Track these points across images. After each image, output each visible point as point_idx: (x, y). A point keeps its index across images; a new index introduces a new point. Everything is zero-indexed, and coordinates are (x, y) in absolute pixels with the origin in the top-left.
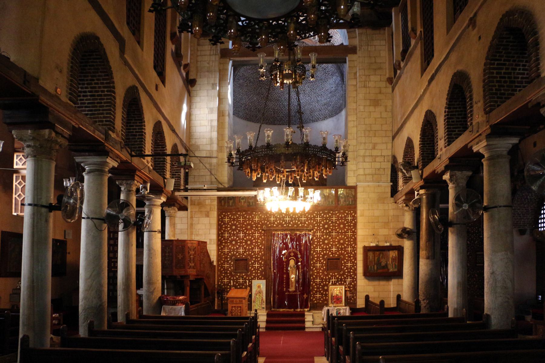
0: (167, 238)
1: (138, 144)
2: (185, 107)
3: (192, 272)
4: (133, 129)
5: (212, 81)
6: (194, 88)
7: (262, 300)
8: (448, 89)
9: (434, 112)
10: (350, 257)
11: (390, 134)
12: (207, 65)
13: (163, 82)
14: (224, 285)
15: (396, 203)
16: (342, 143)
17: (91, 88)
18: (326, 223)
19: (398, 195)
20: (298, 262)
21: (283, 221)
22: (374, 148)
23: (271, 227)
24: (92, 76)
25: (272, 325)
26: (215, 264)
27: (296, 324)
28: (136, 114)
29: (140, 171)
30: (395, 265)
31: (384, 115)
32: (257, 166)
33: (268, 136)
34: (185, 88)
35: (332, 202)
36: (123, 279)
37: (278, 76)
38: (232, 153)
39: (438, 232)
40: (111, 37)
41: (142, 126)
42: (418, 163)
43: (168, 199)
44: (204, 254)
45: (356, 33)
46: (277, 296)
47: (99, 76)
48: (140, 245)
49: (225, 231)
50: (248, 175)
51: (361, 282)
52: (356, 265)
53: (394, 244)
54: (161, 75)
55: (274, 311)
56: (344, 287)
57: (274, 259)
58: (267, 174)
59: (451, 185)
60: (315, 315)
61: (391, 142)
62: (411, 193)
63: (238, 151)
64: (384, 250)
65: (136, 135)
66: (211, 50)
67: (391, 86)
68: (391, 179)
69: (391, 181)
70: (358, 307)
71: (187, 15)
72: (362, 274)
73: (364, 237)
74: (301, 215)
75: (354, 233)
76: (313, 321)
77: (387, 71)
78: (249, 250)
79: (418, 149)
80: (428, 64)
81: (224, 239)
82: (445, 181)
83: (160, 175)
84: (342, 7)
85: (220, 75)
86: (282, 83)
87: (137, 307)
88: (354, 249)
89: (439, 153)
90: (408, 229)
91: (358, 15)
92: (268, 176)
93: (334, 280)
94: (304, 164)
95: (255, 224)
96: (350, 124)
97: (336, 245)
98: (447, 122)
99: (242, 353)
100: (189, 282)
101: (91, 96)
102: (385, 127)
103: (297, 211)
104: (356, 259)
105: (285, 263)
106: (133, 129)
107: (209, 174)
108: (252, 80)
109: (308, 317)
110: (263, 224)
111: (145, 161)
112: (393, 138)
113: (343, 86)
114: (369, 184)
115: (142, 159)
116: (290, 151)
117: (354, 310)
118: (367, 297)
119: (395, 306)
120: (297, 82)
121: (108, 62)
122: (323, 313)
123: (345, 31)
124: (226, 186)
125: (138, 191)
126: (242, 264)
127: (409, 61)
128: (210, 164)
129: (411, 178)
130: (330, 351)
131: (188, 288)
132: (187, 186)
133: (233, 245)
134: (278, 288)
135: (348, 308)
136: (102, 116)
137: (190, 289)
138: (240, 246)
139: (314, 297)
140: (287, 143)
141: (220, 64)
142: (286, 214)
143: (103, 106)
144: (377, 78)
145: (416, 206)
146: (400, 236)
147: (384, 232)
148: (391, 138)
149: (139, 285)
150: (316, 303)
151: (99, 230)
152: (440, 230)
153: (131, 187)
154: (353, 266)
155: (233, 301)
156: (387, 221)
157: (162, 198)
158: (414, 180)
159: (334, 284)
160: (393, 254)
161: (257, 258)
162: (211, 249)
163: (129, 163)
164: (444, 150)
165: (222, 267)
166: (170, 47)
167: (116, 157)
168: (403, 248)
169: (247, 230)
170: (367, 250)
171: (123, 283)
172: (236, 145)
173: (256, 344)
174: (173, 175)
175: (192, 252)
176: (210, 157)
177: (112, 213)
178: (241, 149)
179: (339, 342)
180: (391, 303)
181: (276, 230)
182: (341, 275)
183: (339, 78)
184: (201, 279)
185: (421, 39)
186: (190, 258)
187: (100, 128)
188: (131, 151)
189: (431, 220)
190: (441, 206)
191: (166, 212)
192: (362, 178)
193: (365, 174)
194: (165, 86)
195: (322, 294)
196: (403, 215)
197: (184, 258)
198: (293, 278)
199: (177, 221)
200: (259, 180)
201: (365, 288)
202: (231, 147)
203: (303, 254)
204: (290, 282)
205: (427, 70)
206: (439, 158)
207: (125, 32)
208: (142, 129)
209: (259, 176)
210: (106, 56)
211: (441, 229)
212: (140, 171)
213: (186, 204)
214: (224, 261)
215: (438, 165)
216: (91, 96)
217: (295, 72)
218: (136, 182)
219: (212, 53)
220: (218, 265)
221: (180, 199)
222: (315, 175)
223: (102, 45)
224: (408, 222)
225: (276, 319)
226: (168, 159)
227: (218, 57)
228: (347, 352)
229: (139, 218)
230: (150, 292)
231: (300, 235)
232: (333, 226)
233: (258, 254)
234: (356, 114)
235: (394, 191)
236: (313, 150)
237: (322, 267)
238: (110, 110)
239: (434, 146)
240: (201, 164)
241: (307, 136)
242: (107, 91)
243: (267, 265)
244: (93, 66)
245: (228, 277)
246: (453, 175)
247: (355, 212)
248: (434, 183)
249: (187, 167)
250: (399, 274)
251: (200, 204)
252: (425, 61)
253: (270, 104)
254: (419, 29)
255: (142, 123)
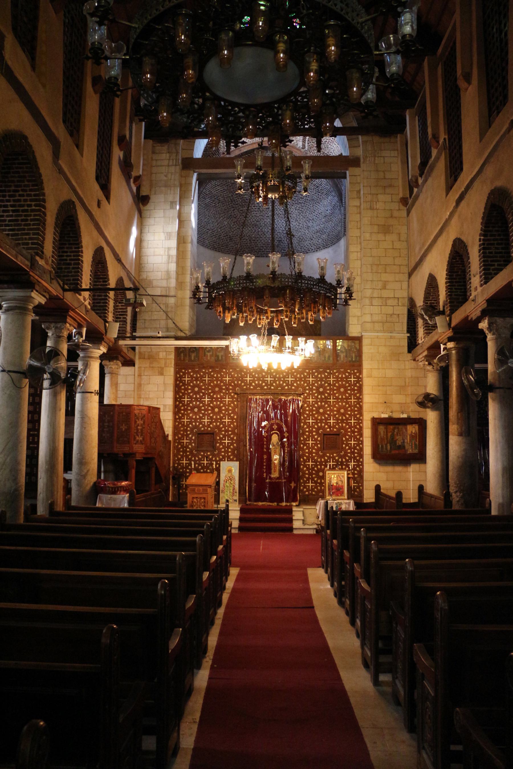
0: (106, 402)
1: (72, 276)
2: (134, 231)
3: (139, 449)
4: (67, 256)
5: (171, 198)
6: (147, 207)
7: (234, 489)
8: (483, 210)
9: (465, 241)
10: (354, 432)
11: (406, 270)
12: (165, 178)
13: (108, 198)
14: (183, 468)
15: (414, 360)
16: (346, 275)
17: (14, 201)
18: (321, 386)
19: (418, 350)
20: (283, 437)
21: (264, 381)
22: (384, 288)
23: (247, 389)
24: (16, 186)
25: (248, 525)
26: (170, 438)
27: (282, 525)
28: (72, 237)
29: (73, 310)
30: (415, 444)
31: (397, 245)
32: (233, 303)
33: (248, 263)
34: (134, 207)
35: (329, 357)
36: (46, 457)
37: (261, 188)
38: (200, 285)
39: (474, 398)
40: (43, 137)
41: (79, 252)
42: (444, 307)
43: (109, 349)
44: (156, 425)
45: (358, 141)
46: (254, 485)
47: (25, 186)
48: (70, 413)
49: (184, 394)
50: (220, 315)
51: (370, 466)
52: (362, 444)
53: (413, 416)
54: (106, 188)
55: (250, 505)
56: (346, 472)
57: (250, 433)
58: (245, 314)
59: (489, 336)
60: (307, 512)
61: (407, 279)
62: (435, 347)
63: (208, 282)
64: (399, 424)
65: (70, 264)
66: (169, 160)
67: (405, 208)
68: (408, 328)
69: (408, 332)
70: (365, 501)
71: (152, 98)
72: (370, 456)
73: (374, 404)
74: (288, 374)
75: (359, 400)
76: (303, 520)
77: (401, 189)
78: (216, 419)
79: (445, 289)
80: (456, 180)
81: (184, 405)
82: (482, 331)
83: (100, 317)
84: (355, 89)
85: (181, 190)
86: (265, 198)
87: (65, 496)
88: (360, 422)
89: (473, 294)
90: (432, 396)
91: (373, 102)
92: (247, 316)
93: (331, 463)
94: (295, 302)
95: (225, 385)
96: (353, 256)
97: (334, 416)
98: (483, 253)
99: (211, 557)
100: (135, 463)
101: (13, 211)
102: (398, 261)
103: (283, 368)
104: (361, 435)
105: (265, 439)
106: (67, 256)
107: (164, 317)
108: (222, 199)
109: (298, 514)
110: (236, 386)
111: (81, 298)
112: (410, 275)
113: (342, 208)
114: (379, 334)
115: (77, 295)
116: (277, 284)
117: (359, 504)
118: (378, 488)
119: (416, 500)
120: (286, 197)
121: (38, 168)
122: (318, 508)
123: (344, 138)
124: (188, 333)
125: (70, 337)
126: (207, 439)
127: (429, 176)
128: (167, 305)
129: (435, 326)
130: (330, 560)
131: (133, 471)
132: (134, 334)
133: (196, 414)
134: (256, 473)
135: (352, 502)
136: (27, 237)
137: (136, 472)
138: (204, 415)
139: (305, 487)
140: (273, 273)
141: (181, 176)
142: (267, 373)
143: (30, 225)
144: (388, 198)
145: (443, 364)
146: (422, 404)
147: (398, 399)
148: (407, 275)
149: (68, 467)
150: (308, 495)
151: (18, 388)
152: (476, 395)
153: (61, 332)
154: (358, 445)
155: (194, 490)
156: (403, 384)
157: (101, 348)
158: (440, 330)
159: (333, 469)
160: (412, 429)
161: (228, 431)
162: (165, 418)
163: (60, 299)
164: (479, 289)
165: (179, 443)
166: (117, 154)
167: (44, 291)
168: (425, 421)
169: (214, 392)
170: (376, 422)
171: (46, 462)
172: (205, 275)
173: (228, 548)
174: (117, 318)
175: (140, 422)
176: (166, 296)
177: (36, 364)
178: (212, 281)
179: (344, 545)
180: (411, 496)
181: (254, 394)
182: (341, 457)
183: (336, 198)
184: (151, 459)
185: (445, 149)
186: (137, 430)
187: (24, 252)
188: (64, 284)
189: (466, 382)
190: (477, 366)
191: (106, 367)
192: (368, 326)
193: (372, 320)
194: (109, 202)
195: (316, 482)
196: (425, 377)
197: (129, 429)
198: (276, 460)
199: (120, 379)
200: (234, 322)
201: (375, 476)
202: (197, 278)
203: (291, 428)
204: (273, 466)
205: (453, 188)
206: (473, 301)
207: (60, 131)
208: (79, 256)
209: (235, 317)
210: (36, 161)
211: (478, 394)
212: (73, 310)
213: (132, 357)
214: (183, 435)
215: (471, 309)
216: (13, 211)
217: (283, 183)
218: (68, 325)
219: (171, 163)
220: (175, 440)
221: (125, 350)
222: (309, 318)
223: (31, 146)
224: (431, 385)
225: (253, 516)
226: (112, 294)
227: (178, 168)
228: (356, 558)
229: (71, 374)
230: (82, 476)
231: (285, 401)
232: (330, 389)
233: (229, 426)
234: (360, 243)
235: (412, 344)
236: (308, 284)
237: (316, 444)
238: (39, 229)
239: (465, 286)
240: (155, 305)
241: (299, 264)
242: (36, 205)
243: (240, 441)
244: (18, 172)
245: (187, 456)
246: (492, 323)
247: (361, 372)
248: (467, 335)
249: (137, 305)
250: (420, 457)
251: (151, 358)
252: (451, 176)
253: (246, 231)
254: (443, 136)
255: (79, 248)
